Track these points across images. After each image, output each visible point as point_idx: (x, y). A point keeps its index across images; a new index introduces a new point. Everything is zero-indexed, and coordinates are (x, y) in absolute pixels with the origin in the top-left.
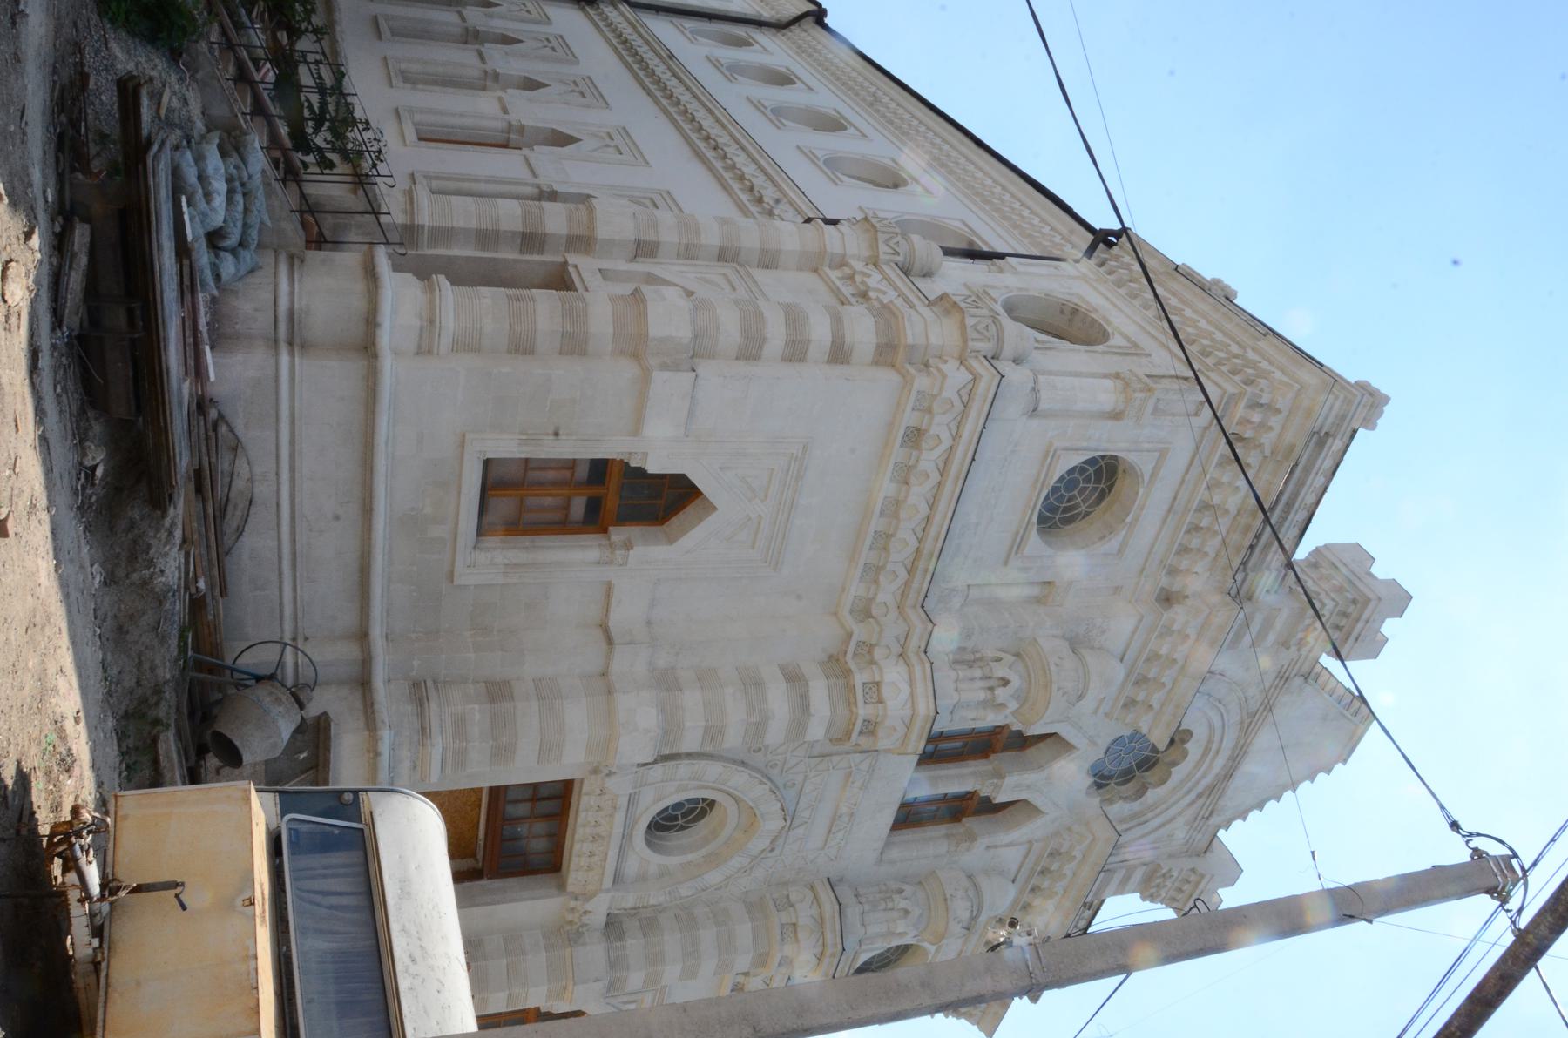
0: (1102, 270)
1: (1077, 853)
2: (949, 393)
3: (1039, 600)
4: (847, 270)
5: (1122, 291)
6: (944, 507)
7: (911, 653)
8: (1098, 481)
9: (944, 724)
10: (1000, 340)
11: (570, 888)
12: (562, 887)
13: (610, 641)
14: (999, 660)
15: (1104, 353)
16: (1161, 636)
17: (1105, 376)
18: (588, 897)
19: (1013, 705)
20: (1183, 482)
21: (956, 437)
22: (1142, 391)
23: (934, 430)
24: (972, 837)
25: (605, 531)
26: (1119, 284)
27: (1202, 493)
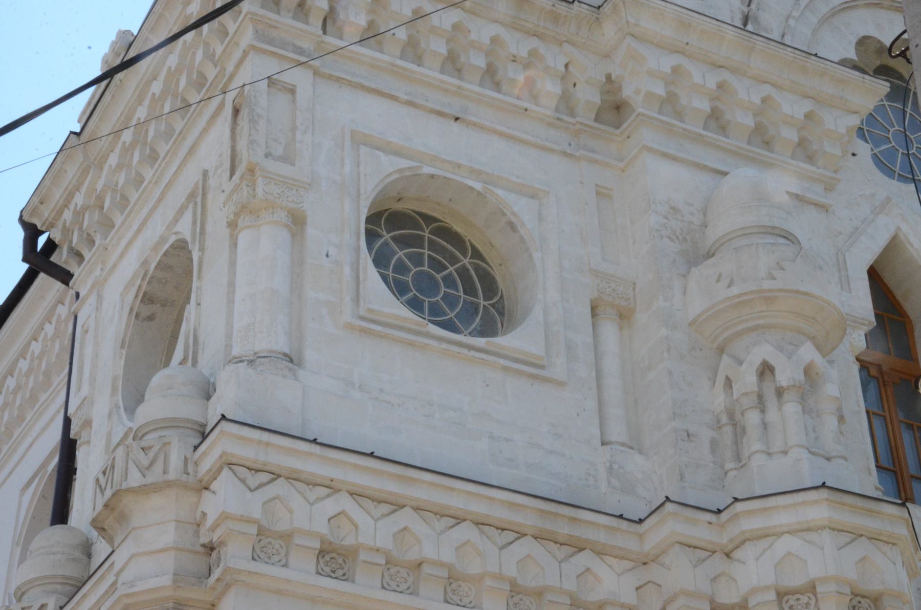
0: (87, 255)
2: (254, 506)
3: (624, 316)
5: (118, 219)
6: (457, 498)
7: (724, 539)
8: (417, 241)
9: (860, 471)
10: (172, 424)
14: (729, 382)
15: (202, 249)
16: (679, 115)
19: (808, 353)
20: (410, 104)
21: (332, 488)
22: (253, 186)
23: (321, 527)
26: (108, 225)
27: (431, 72)
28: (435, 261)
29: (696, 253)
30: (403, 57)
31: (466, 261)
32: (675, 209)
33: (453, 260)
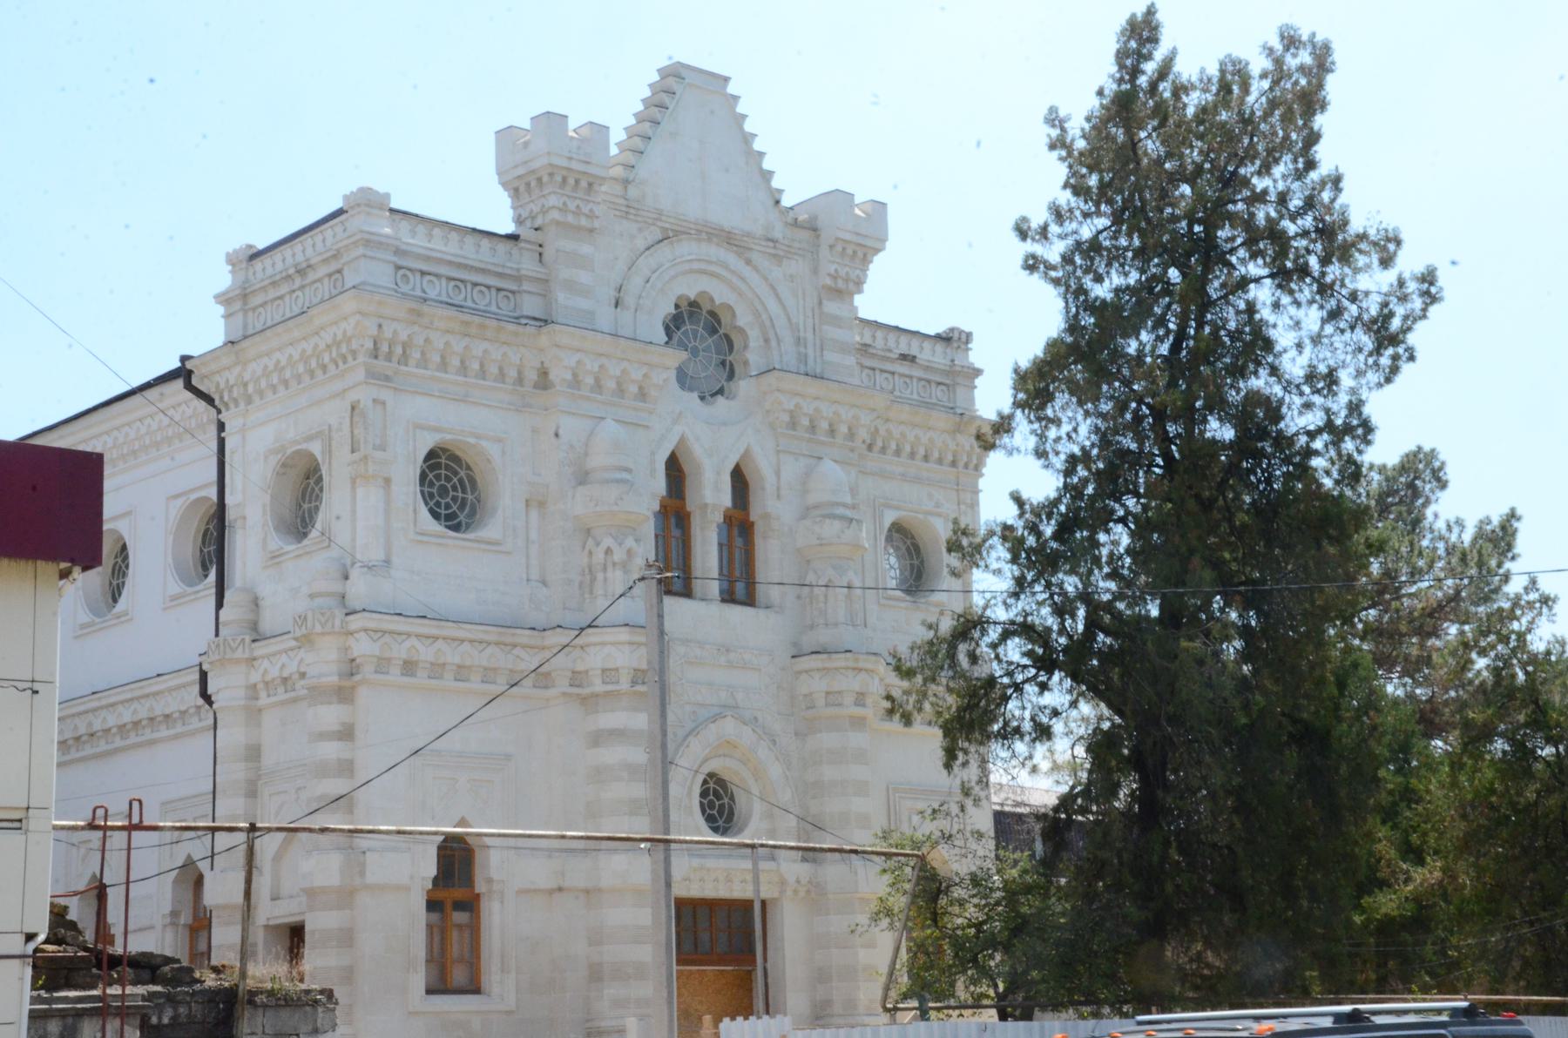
1: (790, 404)
3: (542, 504)
4: (260, 686)
11: (776, 895)
12: (775, 900)
13: (560, 889)
17: (354, 498)
18: (783, 883)
19: (630, 542)
24: (767, 516)
25: (478, 895)
28: (450, 487)
29: (583, 478)
30: (438, 370)
31: (470, 497)
32: (572, 446)
33: (456, 473)
